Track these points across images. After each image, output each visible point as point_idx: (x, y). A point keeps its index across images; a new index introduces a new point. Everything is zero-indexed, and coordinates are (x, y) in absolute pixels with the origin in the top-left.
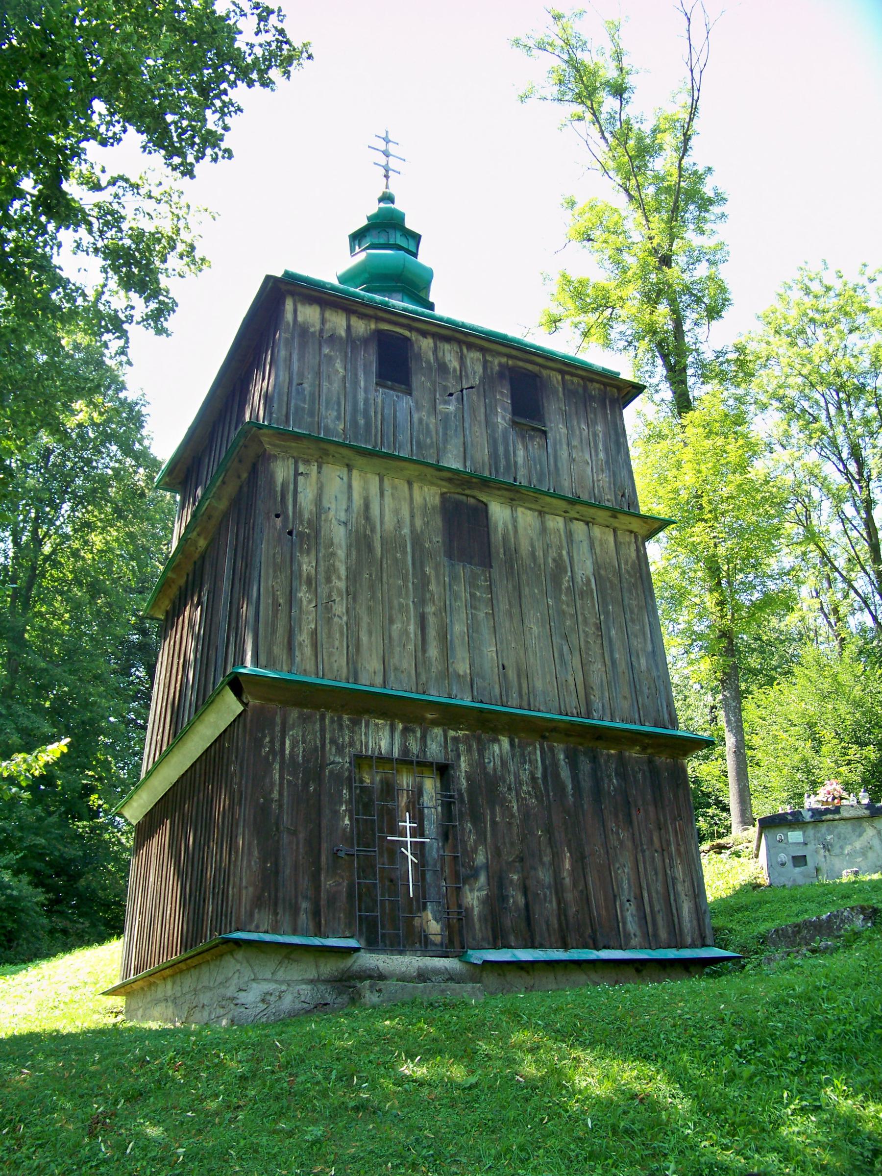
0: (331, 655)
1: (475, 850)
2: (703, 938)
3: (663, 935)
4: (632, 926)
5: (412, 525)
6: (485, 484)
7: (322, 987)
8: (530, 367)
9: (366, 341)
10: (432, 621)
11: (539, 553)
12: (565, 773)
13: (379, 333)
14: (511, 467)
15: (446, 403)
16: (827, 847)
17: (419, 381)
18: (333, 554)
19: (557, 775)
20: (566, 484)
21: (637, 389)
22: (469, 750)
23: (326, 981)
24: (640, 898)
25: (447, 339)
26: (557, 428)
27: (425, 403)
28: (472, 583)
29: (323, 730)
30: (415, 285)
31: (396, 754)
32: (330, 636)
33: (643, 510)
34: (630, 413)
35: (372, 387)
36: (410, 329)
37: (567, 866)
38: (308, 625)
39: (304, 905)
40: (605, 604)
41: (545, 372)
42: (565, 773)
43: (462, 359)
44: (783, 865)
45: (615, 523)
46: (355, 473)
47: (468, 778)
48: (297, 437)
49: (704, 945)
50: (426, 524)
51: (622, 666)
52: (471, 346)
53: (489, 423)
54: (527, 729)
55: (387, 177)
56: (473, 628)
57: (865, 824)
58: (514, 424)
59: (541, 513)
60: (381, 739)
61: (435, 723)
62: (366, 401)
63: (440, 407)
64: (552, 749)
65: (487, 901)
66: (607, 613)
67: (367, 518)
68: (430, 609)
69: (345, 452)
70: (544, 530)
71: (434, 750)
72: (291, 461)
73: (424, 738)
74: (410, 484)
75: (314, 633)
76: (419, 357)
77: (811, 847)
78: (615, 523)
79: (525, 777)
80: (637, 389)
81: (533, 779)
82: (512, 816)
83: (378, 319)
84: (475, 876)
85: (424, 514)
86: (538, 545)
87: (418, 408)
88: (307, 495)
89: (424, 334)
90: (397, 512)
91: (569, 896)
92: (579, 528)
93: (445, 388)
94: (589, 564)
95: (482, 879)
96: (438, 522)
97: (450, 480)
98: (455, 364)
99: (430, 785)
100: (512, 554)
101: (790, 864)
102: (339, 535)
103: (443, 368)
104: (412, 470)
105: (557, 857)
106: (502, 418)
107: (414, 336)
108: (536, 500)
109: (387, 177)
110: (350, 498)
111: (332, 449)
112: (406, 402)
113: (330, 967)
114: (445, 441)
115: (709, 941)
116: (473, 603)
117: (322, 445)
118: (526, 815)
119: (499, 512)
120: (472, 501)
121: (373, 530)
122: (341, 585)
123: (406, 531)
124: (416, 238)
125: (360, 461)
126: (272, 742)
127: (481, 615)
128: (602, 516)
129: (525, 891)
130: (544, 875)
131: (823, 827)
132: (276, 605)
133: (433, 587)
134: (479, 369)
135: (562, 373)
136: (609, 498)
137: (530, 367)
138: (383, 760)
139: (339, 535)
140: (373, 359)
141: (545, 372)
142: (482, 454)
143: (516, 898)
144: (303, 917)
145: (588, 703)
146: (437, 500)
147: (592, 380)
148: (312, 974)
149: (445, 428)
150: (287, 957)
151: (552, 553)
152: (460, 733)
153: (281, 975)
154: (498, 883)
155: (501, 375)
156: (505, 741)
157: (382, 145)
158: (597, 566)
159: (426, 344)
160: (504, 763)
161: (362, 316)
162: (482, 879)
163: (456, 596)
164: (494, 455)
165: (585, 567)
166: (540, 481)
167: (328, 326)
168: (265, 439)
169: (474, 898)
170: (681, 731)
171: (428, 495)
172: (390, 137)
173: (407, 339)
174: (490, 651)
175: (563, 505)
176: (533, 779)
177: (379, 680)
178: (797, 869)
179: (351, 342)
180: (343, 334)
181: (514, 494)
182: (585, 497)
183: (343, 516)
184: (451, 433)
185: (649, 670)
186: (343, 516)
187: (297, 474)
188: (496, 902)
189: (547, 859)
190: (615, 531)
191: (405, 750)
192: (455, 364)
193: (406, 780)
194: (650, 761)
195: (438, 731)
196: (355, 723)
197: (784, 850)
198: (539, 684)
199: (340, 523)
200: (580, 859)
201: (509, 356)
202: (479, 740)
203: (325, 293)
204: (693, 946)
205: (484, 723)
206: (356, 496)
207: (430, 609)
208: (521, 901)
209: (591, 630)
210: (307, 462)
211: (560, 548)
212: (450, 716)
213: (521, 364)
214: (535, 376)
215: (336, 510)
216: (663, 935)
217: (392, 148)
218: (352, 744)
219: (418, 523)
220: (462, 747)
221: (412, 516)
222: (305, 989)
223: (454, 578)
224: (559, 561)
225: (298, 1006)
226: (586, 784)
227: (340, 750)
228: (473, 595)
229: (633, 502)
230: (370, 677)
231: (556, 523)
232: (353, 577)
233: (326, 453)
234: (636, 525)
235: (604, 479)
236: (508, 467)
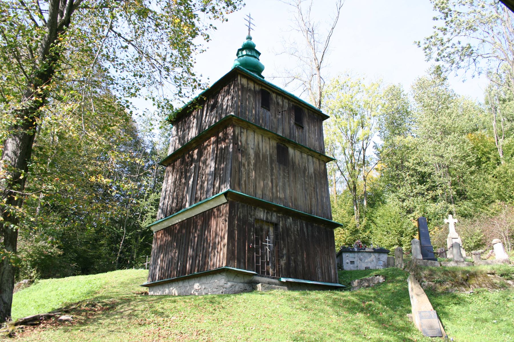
0: (249, 188)
1: (283, 249)
2: (336, 281)
3: (327, 279)
4: (320, 276)
5: (270, 151)
6: (289, 142)
7: (246, 285)
8: (300, 106)
9: (259, 92)
10: (274, 181)
11: (300, 164)
12: (305, 230)
13: (262, 90)
14: (294, 137)
15: (279, 115)
16: (361, 260)
17: (272, 107)
18: (250, 158)
19: (303, 230)
20: (308, 144)
21: (327, 117)
22: (282, 220)
23: (246, 283)
24: (322, 267)
25: (280, 95)
26: (306, 127)
27: (273, 114)
28: (284, 171)
29: (247, 210)
30: (259, 69)
31: (265, 219)
32: (249, 182)
33: (326, 154)
34: (324, 122)
35: (260, 107)
36: (270, 90)
37: (305, 256)
38: (244, 179)
39: (242, 260)
40: (316, 181)
41: (304, 109)
42: (305, 230)
43: (283, 101)
44: (348, 263)
45: (320, 158)
46: (256, 134)
47: (282, 228)
48: (266, 130)
49: (336, 283)
50: (273, 152)
51: (319, 200)
52: (285, 98)
53: (289, 123)
54: (297, 216)
55: (249, 30)
56: (284, 184)
57: (372, 254)
58: (295, 124)
59: (301, 152)
60: (261, 215)
61: (275, 211)
62: (259, 111)
63: (277, 116)
64: (302, 222)
65: (285, 264)
66: (316, 184)
67: (259, 148)
68: (274, 177)
69: (254, 127)
70: (302, 157)
71: (274, 219)
72: (239, 128)
73: (272, 215)
74: (269, 139)
75: (245, 181)
76: (272, 99)
77: (356, 259)
78: (320, 158)
79: (296, 229)
80: (327, 117)
81: (298, 230)
82: (292, 240)
83: (262, 86)
84: (283, 257)
85: (273, 149)
86: (300, 162)
87: (272, 116)
88: (244, 139)
89: (274, 92)
90: (266, 147)
91: (306, 265)
92: (310, 157)
93: (278, 110)
94: (312, 169)
95: (285, 258)
96: (275, 151)
97: (280, 139)
98: (281, 103)
99: (271, 230)
100: (294, 163)
101: (349, 263)
102: (252, 152)
103: (278, 103)
104: (270, 135)
105: (303, 253)
106: (292, 122)
107: (271, 92)
108: (301, 148)
109: (249, 30)
110: (254, 141)
111: (251, 125)
112: (268, 113)
113: (247, 279)
114: (278, 127)
115: (338, 282)
116: (284, 177)
117: (249, 124)
118: (296, 240)
119: (291, 151)
120: (282, 145)
121: (260, 152)
122: (252, 167)
123: (268, 153)
124: (259, 54)
125: (257, 130)
126: (235, 212)
127: (286, 181)
128: (317, 155)
129: (295, 262)
130: (299, 258)
131: (360, 254)
132: (236, 171)
133: (274, 171)
134: (287, 105)
135: (308, 109)
136: (318, 150)
137: (300, 106)
138: (262, 221)
139: (252, 152)
140: (261, 98)
141: (304, 109)
142: (287, 131)
143: (293, 264)
144: (242, 264)
145: (311, 210)
146: (276, 145)
147: (315, 113)
148: (242, 281)
149: (278, 123)
150: (236, 275)
151: (304, 165)
152: (280, 215)
153: (235, 280)
154: (289, 259)
155: (292, 107)
156: (291, 218)
157: (248, 19)
158: (315, 170)
159: (274, 95)
160: (291, 225)
161: (258, 84)
162: (285, 258)
163: (280, 174)
164: (290, 133)
165: (311, 170)
166: (301, 142)
167: (249, 86)
168: (234, 120)
169: (283, 262)
170: (333, 221)
171: (274, 143)
172: (251, 17)
173: (269, 93)
174: (288, 192)
175: (307, 150)
176: (298, 230)
177: (261, 197)
178: (352, 265)
179: (255, 92)
180: (253, 89)
181: (296, 146)
182: (312, 149)
183: (252, 147)
184: (280, 124)
185: (326, 202)
186: (252, 147)
187: (241, 132)
188: (288, 264)
189: (300, 254)
190: (319, 160)
191: (267, 218)
192: (281, 103)
193: (265, 227)
194: (325, 229)
195: (275, 214)
196: (255, 209)
197: (348, 259)
198: (299, 203)
199: (252, 148)
200: (308, 255)
201: (295, 102)
202: (285, 218)
203: (301, 105)
204: (334, 283)
205: (286, 212)
206: (256, 141)
207: (274, 177)
208: (294, 265)
209: (312, 189)
210: (244, 128)
211: (305, 163)
212: (279, 210)
213: (267, 90)
214: (301, 109)
215: (251, 145)
216: (327, 279)
217: (252, 21)
218: (254, 215)
219: (271, 151)
220: (281, 219)
221: (270, 149)
222: (241, 285)
223: (280, 169)
224: (305, 167)
225: (240, 289)
226: (310, 233)
227: (251, 217)
228: (284, 175)
229: (324, 152)
230: (259, 197)
231: (305, 156)
232: (255, 165)
233: (249, 126)
234: (325, 159)
235: (317, 143)
236: (293, 137)
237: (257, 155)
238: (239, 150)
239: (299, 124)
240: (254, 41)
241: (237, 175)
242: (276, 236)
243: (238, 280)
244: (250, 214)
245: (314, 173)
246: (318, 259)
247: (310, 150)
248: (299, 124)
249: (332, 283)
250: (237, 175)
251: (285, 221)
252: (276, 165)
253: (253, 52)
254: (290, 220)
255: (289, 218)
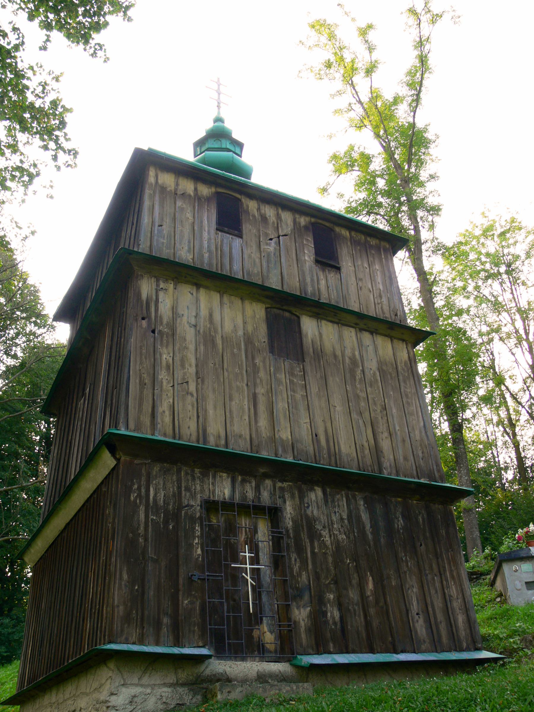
7: (180, 690)
8: (327, 224)
12: (365, 517)
13: (217, 193)
17: (247, 228)
23: (183, 685)
26: (346, 263)
54: (335, 480)
55: (218, 107)
58: (317, 262)
61: (266, 476)
76: (247, 212)
82: (326, 547)
83: (217, 185)
89: (251, 197)
93: (266, 235)
103: (264, 219)
109: (218, 107)
113: (183, 675)
121: (216, 331)
123: (240, 333)
124: (240, 145)
126: (139, 488)
127: (298, 396)
129: (340, 606)
130: (353, 594)
132: (142, 384)
137: (327, 224)
138: (227, 506)
152: (285, 485)
181: (325, 311)
204: (468, 649)
205: (303, 475)
208: (337, 614)
212: (279, 470)
215: (187, 316)
222: (166, 691)
228: (291, 382)
237: (236, 344)
238: (153, 332)
239: (327, 260)
240: (228, 125)
241: (148, 392)
242: (277, 542)
243: (156, 678)
244: (187, 489)
245: (380, 370)
246: (413, 593)
247: (360, 316)
248: (327, 260)
249: (461, 650)
250: (148, 392)
251: (302, 498)
252: (264, 361)
253: (223, 141)
254: (316, 495)
255: (312, 489)
